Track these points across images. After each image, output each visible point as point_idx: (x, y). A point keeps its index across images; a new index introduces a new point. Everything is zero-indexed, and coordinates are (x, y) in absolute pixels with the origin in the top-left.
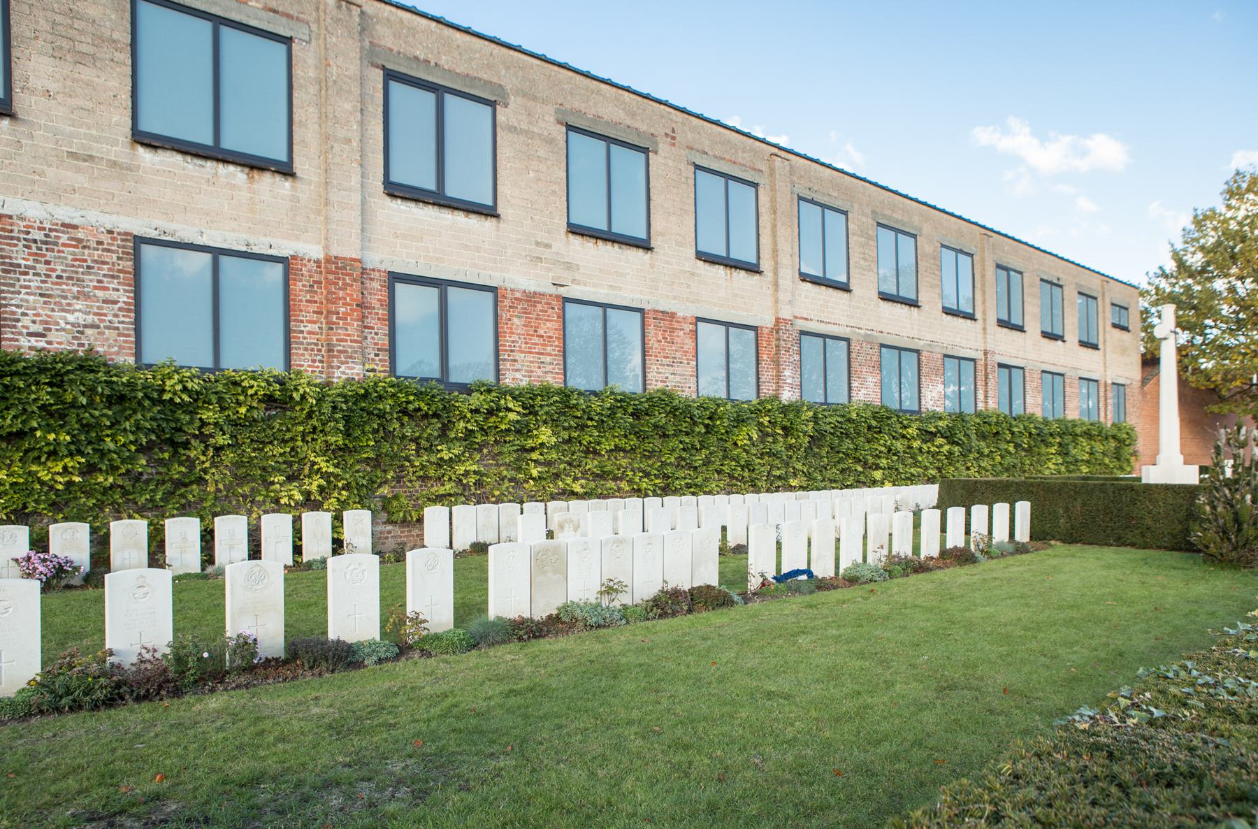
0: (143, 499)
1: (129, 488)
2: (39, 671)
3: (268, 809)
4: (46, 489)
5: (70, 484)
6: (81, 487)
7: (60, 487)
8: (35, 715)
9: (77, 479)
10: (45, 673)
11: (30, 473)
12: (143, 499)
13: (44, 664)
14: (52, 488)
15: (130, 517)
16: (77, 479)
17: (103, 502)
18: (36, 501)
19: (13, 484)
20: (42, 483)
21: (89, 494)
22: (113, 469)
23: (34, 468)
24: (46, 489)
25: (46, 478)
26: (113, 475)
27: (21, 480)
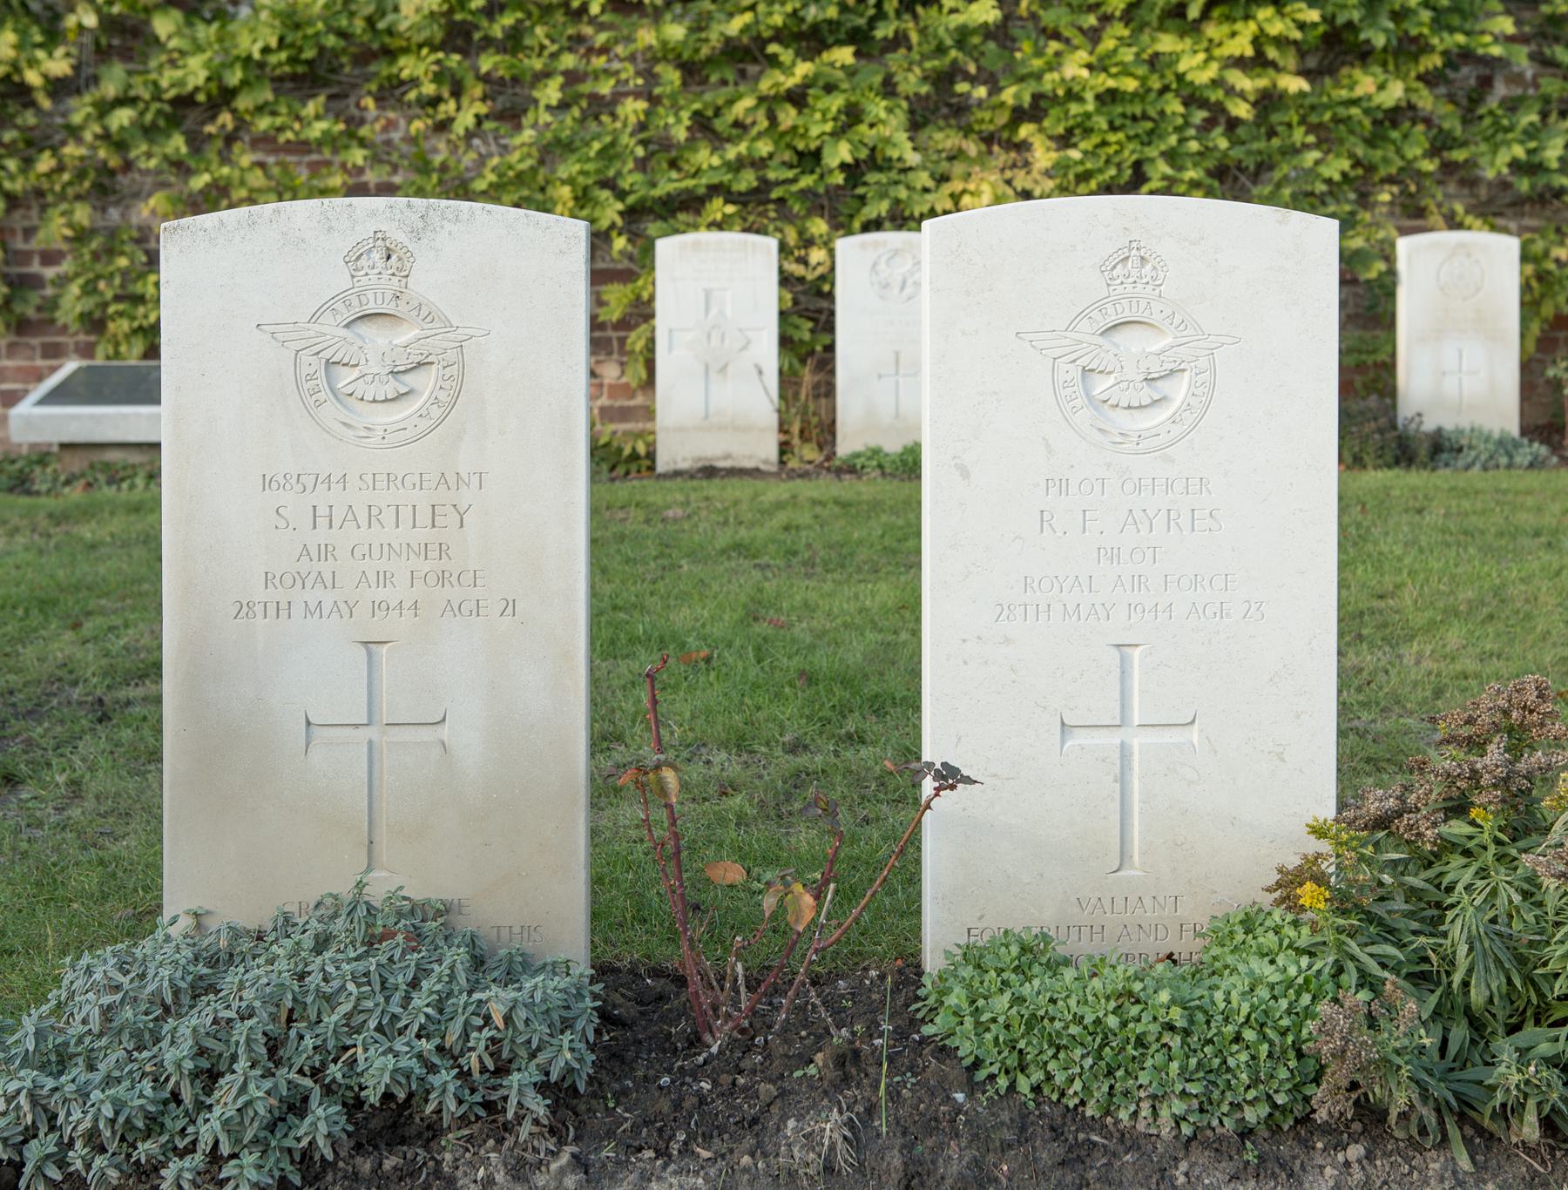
0: (1503, 158)
1: (1453, 124)
2: (1328, 811)
3: (344, 60)
4: (1200, 116)
5: (1268, 101)
6: (1307, 108)
7: (1242, 110)
8: (1337, 1135)
9: (1294, 84)
10: (1367, 825)
11: (1154, 62)
12: (1503, 158)
13: (1362, 754)
14: (1218, 110)
15: (1453, 223)
16: (1294, 84)
17: (1371, 169)
18: (1171, 156)
19: (1109, 98)
20: (1193, 99)
21: (1326, 139)
22: (1407, 49)
23: (1167, 43)
24: (1200, 116)
25: (1203, 77)
26: (1399, 74)
27: (1130, 85)
